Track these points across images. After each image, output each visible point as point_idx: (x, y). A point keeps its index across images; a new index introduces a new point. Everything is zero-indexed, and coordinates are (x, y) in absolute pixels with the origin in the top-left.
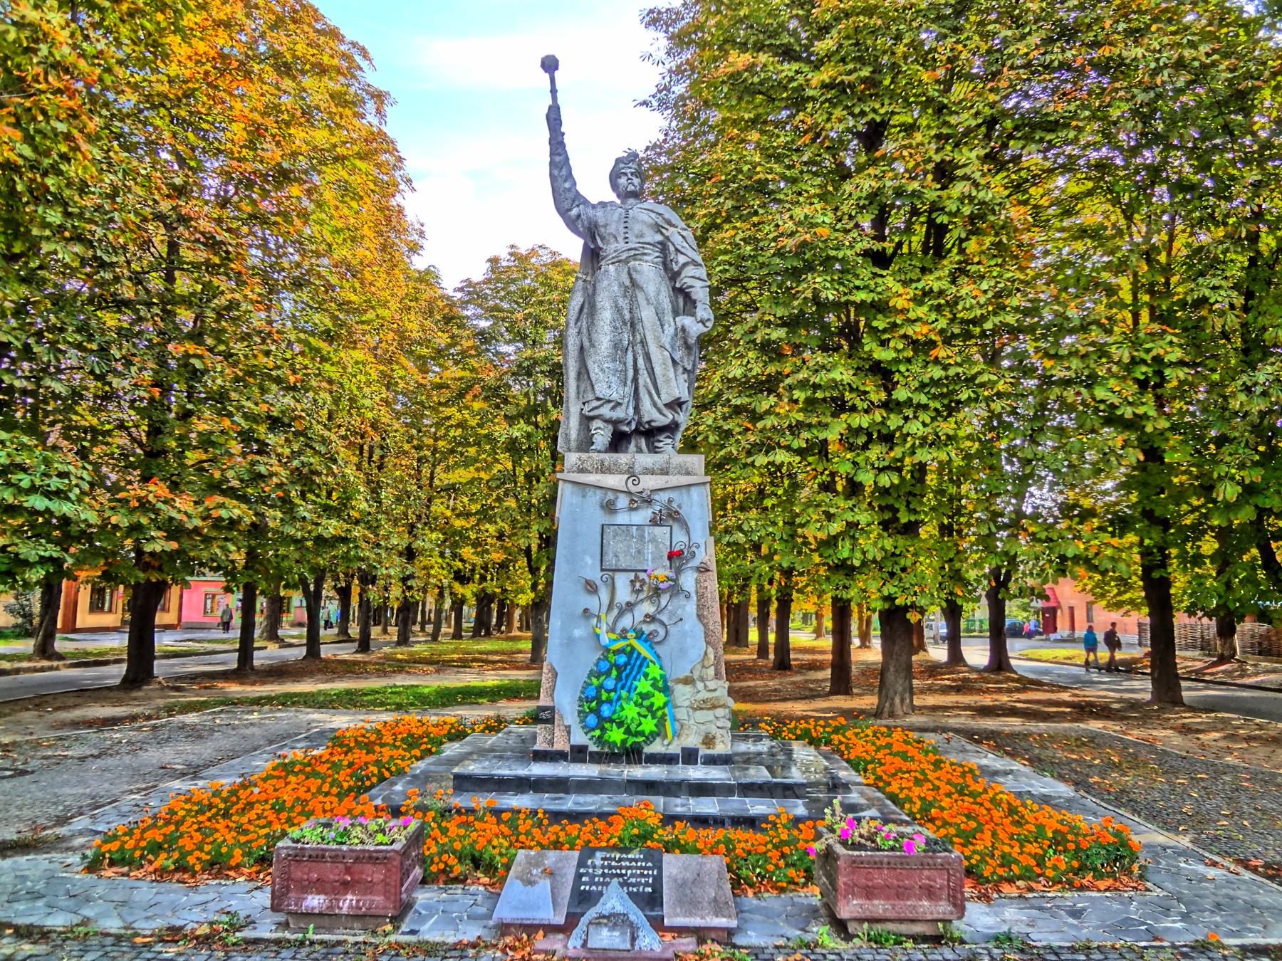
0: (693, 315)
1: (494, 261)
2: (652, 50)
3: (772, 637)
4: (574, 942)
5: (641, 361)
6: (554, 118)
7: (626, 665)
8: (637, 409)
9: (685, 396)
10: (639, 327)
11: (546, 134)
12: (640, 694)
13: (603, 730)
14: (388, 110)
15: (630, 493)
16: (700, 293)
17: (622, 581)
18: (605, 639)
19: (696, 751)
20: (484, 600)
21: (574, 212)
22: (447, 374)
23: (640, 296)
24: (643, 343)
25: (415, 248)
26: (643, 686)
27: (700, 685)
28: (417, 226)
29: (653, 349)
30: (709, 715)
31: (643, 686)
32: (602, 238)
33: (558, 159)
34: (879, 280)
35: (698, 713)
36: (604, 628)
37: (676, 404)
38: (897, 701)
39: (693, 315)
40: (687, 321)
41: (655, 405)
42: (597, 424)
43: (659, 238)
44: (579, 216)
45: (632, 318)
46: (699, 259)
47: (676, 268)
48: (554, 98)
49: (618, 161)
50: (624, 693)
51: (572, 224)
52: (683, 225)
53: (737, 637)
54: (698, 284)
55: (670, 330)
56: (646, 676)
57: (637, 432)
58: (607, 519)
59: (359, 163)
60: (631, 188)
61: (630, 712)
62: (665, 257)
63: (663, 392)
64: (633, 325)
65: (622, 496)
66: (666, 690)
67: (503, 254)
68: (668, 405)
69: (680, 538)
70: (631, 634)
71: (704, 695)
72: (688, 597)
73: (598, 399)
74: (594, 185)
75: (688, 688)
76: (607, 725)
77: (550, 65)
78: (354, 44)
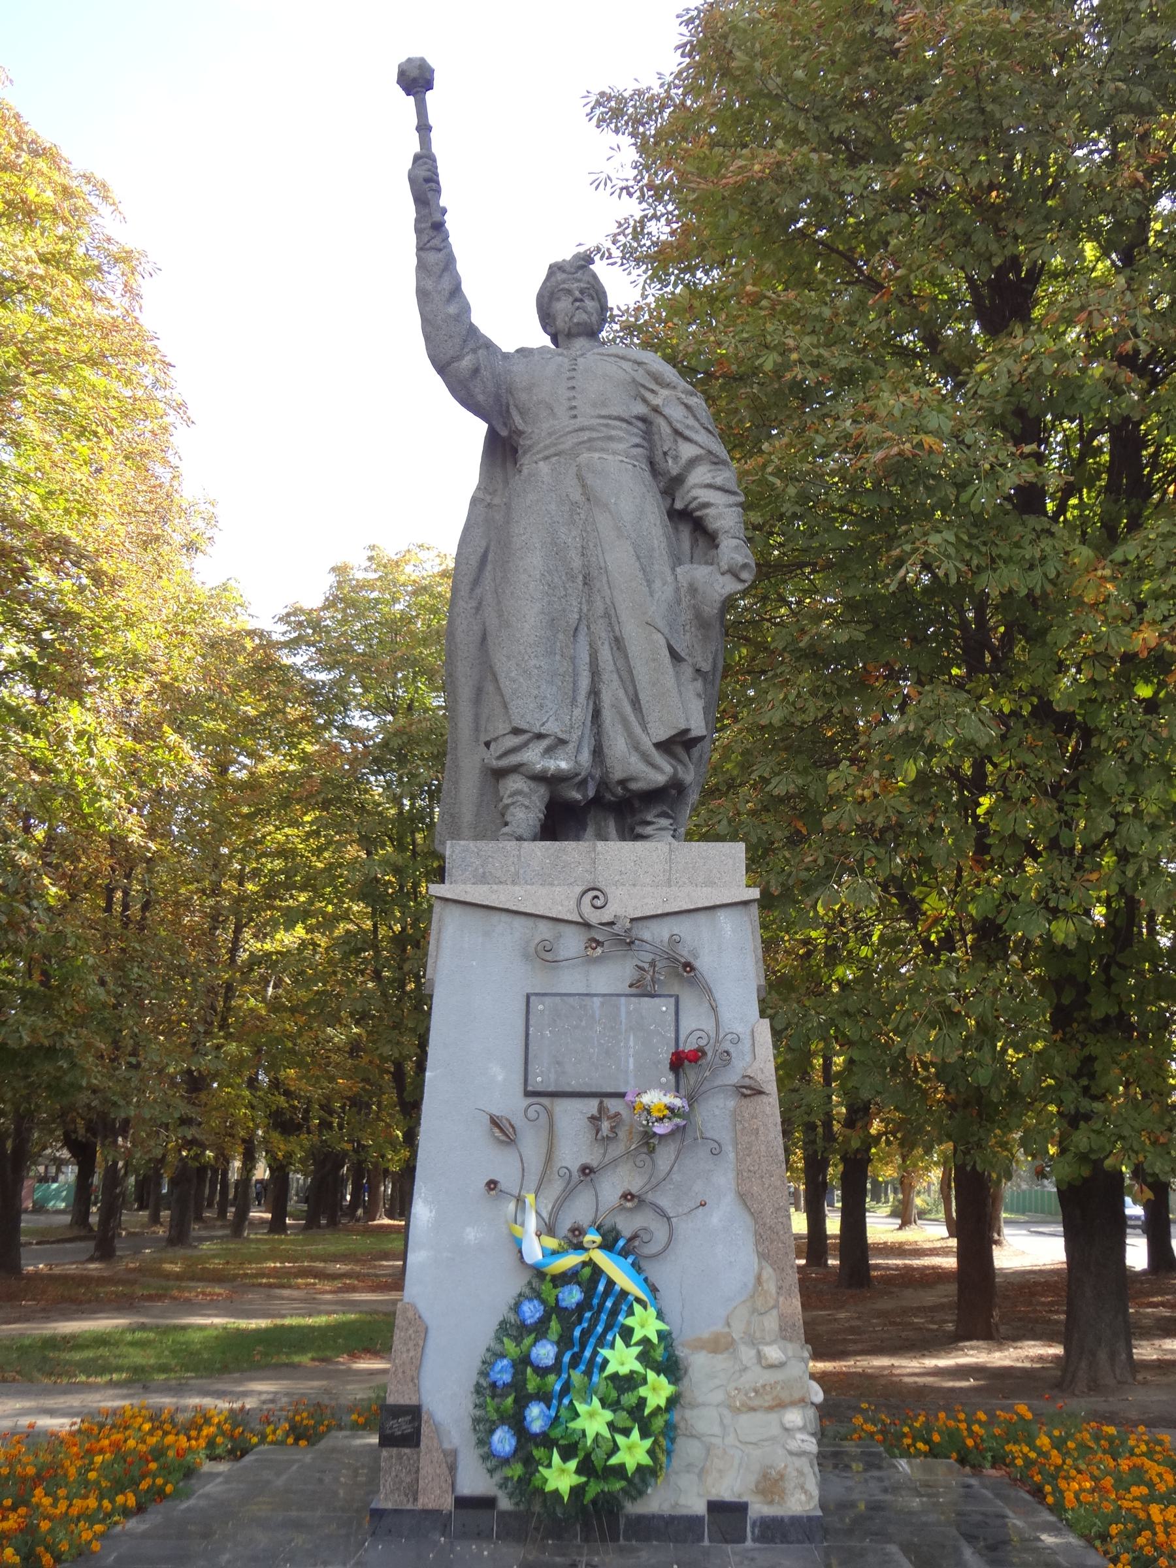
2: (609, 169)
3: (833, 1225)
6: (425, 183)
7: (581, 1307)
8: (598, 752)
9: (698, 727)
11: (408, 210)
12: (615, 1377)
13: (530, 1464)
14: (146, 286)
15: (587, 925)
16: (725, 515)
17: (572, 1117)
18: (534, 1251)
19: (740, 1509)
20: (326, 1166)
21: (466, 362)
22: (262, 769)
24: (610, 616)
26: (621, 1359)
27: (747, 1354)
29: (631, 630)
31: (621, 1359)
33: (432, 257)
35: (745, 1419)
36: (532, 1223)
37: (679, 744)
38: (1103, 1355)
40: (701, 573)
41: (636, 747)
42: (515, 783)
43: (640, 409)
44: (476, 371)
47: (675, 470)
50: (577, 1376)
51: (465, 390)
52: (683, 384)
55: (664, 592)
56: (627, 1333)
57: (597, 802)
59: (87, 371)
60: (580, 317)
61: (593, 1420)
62: (651, 448)
63: (652, 717)
64: (587, 581)
65: (569, 931)
66: (671, 1368)
69: (695, 1025)
70: (592, 1237)
71: (757, 1376)
73: (516, 731)
74: (509, 321)
75: (721, 1362)
76: (538, 1453)
77: (416, 80)
78: (88, 179)
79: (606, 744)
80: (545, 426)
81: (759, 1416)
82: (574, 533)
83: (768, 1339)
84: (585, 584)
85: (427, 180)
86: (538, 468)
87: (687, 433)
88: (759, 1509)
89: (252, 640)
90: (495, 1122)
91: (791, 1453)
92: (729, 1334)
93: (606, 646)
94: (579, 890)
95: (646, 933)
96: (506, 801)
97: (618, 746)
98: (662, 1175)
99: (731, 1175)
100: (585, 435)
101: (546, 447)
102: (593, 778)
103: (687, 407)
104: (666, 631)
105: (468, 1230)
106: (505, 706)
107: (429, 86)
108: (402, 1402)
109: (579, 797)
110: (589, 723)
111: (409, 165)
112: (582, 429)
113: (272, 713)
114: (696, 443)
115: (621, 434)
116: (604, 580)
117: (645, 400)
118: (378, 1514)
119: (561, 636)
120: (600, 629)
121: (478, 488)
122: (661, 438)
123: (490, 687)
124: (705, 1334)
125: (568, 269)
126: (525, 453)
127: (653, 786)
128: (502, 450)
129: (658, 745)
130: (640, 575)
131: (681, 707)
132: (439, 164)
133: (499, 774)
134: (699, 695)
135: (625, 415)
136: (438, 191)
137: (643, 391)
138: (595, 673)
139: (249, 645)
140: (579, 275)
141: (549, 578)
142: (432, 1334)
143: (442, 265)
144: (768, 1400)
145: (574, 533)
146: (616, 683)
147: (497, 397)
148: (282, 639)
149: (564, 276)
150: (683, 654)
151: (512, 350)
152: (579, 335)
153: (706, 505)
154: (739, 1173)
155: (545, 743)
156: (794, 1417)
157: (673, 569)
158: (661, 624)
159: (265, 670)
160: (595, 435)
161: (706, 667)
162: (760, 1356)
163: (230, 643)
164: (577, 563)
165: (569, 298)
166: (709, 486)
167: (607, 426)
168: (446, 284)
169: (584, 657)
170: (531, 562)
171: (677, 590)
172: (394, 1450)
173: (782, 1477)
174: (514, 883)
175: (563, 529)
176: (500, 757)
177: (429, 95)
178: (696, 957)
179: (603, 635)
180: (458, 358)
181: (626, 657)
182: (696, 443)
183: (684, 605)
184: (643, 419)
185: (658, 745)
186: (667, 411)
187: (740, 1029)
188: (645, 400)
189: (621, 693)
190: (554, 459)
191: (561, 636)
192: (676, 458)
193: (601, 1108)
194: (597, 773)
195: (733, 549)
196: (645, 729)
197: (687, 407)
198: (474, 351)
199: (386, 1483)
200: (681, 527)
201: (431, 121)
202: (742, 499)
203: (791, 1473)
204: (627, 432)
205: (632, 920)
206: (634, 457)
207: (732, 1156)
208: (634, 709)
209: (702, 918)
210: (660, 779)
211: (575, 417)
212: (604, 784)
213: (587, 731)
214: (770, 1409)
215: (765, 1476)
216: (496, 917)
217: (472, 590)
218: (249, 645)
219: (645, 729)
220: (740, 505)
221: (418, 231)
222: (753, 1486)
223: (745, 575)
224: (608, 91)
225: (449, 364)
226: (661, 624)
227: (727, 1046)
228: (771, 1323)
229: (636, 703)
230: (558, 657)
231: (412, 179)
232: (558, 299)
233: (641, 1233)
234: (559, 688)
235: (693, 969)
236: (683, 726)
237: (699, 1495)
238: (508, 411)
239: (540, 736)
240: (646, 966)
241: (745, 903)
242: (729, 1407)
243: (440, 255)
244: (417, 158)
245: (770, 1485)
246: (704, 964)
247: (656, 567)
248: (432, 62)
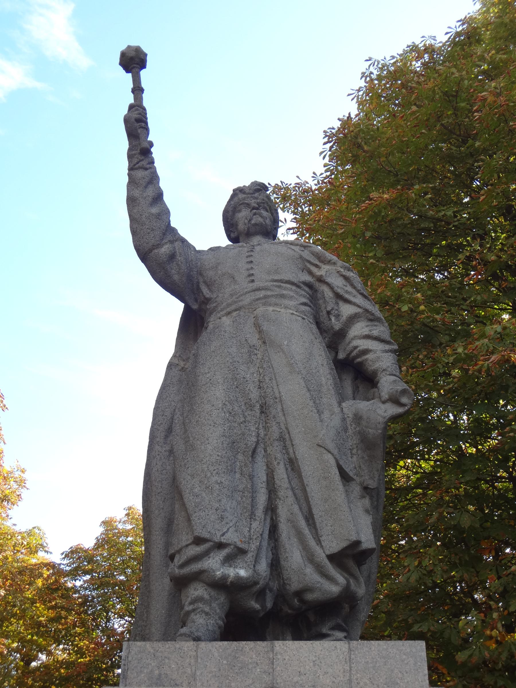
5: (281, 473)
6: (136, 124)
8: (275, 565)
9: (368, 540)
11: (122, 143)
16: (381, 358)
21: (165, 250)
23: (278, 361)
24: (285, 440)
28: (17, 474)
29: (304, 451)
32: (209, 285)
33: (140, 174)
37: (350, 557)
41: (311, 558)
42: (197, 590)
44: (172, 257)
45: (263, 397)
47: (337, 326)
63: (326, 527)
64: (264, 410)
74: (201, 227)
77: (133, 61)
82: (252, 370)
84: (262, 412)
85: (138, 121)
86: (222, 324)
87: (347, 296)
89: (48, 570)
93: (282, 466)
96: (187, 608)
97: (294, 558)
100: (262, 294)
101: (229, 305)
102: (271, 590)
103: (346, 278)
104: (335, 452)
106: (189, 520)
109: (257, 606)
111: (126, 112)
112: (258, 289)
113: (57, 619)
114: (354, 304)
115: (292, 294)
116: (279, 407)
117: (310, 273)
119: (240, 457)
120: (276, 450)
121: (174, 356)
122: (325, 302)
123: (180, 518)
125: (247, 191)
126: (211, 313)
128: (192, 325)
129: (331, 558)
130: (311, 403)
131: (352, 522)
133: (181, 583)
134: (367, 511)
135: (295, 281)
137: (308, 265)
138: (272, 490)
139: (46, 573)
140: (256, 195)
141: (229, 407)
143: (147, 179)
145: (252, 370)
146: (291, 499)
147: (190, 278)
148: (68, 568)
149: (244, 196)
150: (351, 474)
152: (256, 234)
153: (366, 352)
155: (225, 552)
157: (340, 404)
158: (331, 446)
159: (54, 590)
160: (269, 293)
161: (372, 484)
163: (32, 570)
164: (254, 394)
165: (250, 212)
166: (368, 337)
168: (150, 192)
169: (262, 476)
170: (215, 395)
171: (344, 419)
175: (243, 367)
177: (143, 73)
179: (279, 455)
180: (158, 246)
181: (300, 477)
182: (354, 304)
183: (350, 432)
184: (310, 286)
186: (329, 280)
188: (310, 273)
189: (296, 508)
190: (235, 314)
191: (240, 457)
192: (338, 316)
194: (275, 585)
196: (319, 542)
197: (346, 278)
198: (171, 242)
200: (344, 377)
201: (144, 85)
202: (396, 347)
204: (297, 293)
206: (303, 312)
208: (308, 525)
210: (335, 589)
211: (253, 281)
212: (281, 596)
213: (265, 543)
217: (166, 437)
218: (46, 573)
219: (319, 542)
220: (394, 351)
221: (130, 157)
223: (404, 400)
224: (280, 184)
225: (151, 251)
226: (331, 446)
229: (310, 518)
230: (238, 476)
231: (127, 120)
232: (240, 211)
234: (239, 503)
236: (354, 538)
238: (198, 286)
239: (220, 546)
243: (147, 173)
244: (131, 107)
247: (325, 400)
248: (145, 50)
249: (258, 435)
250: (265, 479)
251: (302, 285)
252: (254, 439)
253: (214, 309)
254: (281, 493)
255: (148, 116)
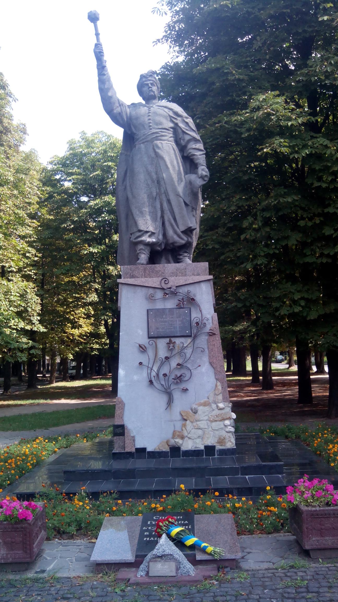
0: (196, 173)
1: (71, 143)
4: (141, 573)
6: (99, 54)
10: (162, 183)
11: (95, 62)
15: (163, 289)
24: (166, 193)
25: (21, 141)
30: (221, 424)
34: (315, 140)
35: (214, 424)
39: (196, 173)
40: (193, 177)
41: (175, 232)
43: (172, 125)
46: (198, 137)
48: (98, 39)
49: (142, 77)
53: (238, 369)
54: (198, 153)
58: (150, 307)
64: (158, 182)
67: (77, 138)
68: (184, 232)
71: (217, 412)
72: (203, 351)
75: (207, 408)
77: (93, 18)
79: (167, 233)
80: (142, 132)
81: (218, 423)
83: (219, 402)
84: (158, 183)
87: (187, 132)
88: (218, 447)
90: (140, 346)
91: (227, 432)
92: (208, 401)
94: (160, 278)
95: (182, 290)
96: (138, 252)
97: (170, 232)
98: (188, 358)
99: (207, 357)
101: (143, 139)
105: (135, 376)
107: (97, 19)
108: (119, 424)
109: (159, 249)
110: (161, 226)
111: (93, 47)
118: (114, 454)
124: (202, 401)
127: (181, 244)
129: (182, 232)
132: (103, 46)
136: (103, 56)
138: (162, 211)
142: (126, 405)
144: (220, 418)
151: (129, 104)
154: (209, 357)
155: (149, 234)
156: (227, 422)
160: (158, 135)
162: (217, 406)
164: (155, 177)
167: (161, 132)
169: (158, 206)
172: (118, 437)
173: (224, 438)
174: (142, 277)
176: (135, 239)
178: (195, 296)
185: (182, 232)
187: (209, 316)
192: (184, 140)
193: (170, 341)
195: (203, 170)
196: (178, 227)
199: (116, 446)
203: (227, 437)
205: (176, 287)
207: (207, 352)
209: (197, 285)
210: (183, 242)
212: (167, 244)
213: (161, 229)
214: (221, 421)
215: (220, 438)
216: (137, 288)
217: (123, 183)
219: (178, 227)
221: (98, 68)
222: (216, 441)
227: (205, 321)
228: (220, 397)
232: (144, 87)
233: (183, 375)
235: (194, 300)
237: (202, 444)
240: (181, 300)
241: (209, 280)
242: (209, 421)
244: (96, 45)
245: (221, 441)
246: (198, 298)
249: (157, 192)
250: (159, 207)
251: (170, 129)
252: (155, 194)
253: (138, 139)
254: (165, 212)
255: (103, 49)
